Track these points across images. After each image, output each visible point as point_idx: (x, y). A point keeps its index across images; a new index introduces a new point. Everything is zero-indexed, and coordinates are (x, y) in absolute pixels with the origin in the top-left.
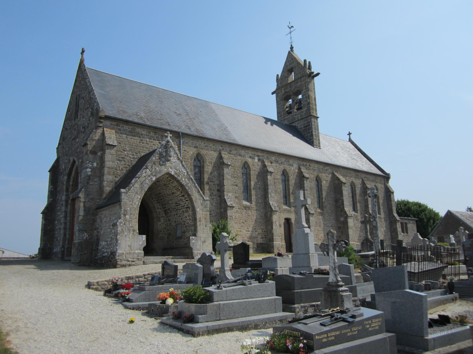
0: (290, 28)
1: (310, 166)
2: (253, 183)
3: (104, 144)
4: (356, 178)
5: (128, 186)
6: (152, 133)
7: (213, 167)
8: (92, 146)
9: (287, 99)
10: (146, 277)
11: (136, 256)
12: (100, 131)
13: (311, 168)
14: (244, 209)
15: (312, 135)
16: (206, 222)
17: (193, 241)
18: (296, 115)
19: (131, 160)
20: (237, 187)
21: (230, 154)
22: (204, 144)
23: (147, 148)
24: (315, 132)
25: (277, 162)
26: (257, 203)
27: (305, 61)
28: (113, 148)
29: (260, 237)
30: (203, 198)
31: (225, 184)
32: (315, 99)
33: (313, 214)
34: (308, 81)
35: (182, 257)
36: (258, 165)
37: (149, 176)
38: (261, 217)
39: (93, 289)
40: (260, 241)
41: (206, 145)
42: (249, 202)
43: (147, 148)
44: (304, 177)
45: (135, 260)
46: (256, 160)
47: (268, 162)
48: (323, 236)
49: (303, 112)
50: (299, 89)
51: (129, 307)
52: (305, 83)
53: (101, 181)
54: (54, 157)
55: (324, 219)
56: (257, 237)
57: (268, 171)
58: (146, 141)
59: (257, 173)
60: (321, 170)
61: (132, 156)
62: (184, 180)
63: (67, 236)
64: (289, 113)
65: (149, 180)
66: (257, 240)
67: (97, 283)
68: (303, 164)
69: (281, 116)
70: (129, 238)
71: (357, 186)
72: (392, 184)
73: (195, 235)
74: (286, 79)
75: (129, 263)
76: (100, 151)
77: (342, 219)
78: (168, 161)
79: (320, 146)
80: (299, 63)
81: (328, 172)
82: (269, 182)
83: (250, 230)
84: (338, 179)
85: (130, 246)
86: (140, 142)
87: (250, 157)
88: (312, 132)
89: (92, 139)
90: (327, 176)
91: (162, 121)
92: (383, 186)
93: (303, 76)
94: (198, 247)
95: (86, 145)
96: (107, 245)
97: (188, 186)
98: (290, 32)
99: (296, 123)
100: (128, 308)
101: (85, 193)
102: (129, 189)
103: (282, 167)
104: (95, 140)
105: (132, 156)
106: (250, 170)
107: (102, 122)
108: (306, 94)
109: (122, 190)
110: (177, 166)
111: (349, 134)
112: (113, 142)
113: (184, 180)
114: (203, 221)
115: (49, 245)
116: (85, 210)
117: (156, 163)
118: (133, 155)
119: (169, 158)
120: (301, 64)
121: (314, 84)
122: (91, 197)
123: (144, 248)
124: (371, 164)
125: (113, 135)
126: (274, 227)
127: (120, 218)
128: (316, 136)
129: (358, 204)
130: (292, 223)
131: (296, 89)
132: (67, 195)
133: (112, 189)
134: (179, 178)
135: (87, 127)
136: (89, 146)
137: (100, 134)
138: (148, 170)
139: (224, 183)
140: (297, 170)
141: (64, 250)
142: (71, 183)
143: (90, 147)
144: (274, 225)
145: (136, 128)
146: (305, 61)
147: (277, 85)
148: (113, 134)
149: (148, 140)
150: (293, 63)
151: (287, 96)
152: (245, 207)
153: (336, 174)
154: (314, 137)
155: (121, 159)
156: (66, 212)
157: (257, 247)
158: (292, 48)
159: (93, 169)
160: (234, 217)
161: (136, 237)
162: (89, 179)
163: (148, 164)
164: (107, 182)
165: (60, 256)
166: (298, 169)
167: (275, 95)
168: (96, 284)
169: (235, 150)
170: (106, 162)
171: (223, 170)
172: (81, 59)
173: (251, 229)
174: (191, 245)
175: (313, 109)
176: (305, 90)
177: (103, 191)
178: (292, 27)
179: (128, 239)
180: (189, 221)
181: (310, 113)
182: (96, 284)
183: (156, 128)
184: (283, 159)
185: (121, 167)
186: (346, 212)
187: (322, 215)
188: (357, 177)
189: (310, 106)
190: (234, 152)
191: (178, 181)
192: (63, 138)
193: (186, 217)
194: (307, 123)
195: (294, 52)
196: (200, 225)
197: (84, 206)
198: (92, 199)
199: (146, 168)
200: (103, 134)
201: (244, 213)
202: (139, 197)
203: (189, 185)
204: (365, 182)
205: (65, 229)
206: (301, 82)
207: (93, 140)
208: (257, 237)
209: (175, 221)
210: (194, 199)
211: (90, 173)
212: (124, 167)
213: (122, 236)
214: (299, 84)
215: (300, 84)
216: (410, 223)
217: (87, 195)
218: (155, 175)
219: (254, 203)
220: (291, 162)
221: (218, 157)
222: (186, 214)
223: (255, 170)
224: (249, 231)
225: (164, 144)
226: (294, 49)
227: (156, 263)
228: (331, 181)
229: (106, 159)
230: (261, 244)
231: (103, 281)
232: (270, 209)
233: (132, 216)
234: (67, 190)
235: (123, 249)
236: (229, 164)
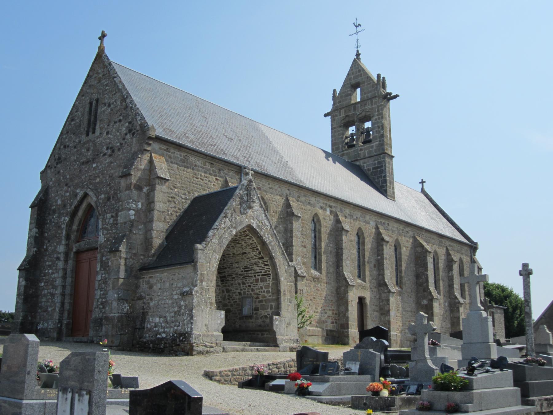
0: (357, 27)
1: (388, 225)
2: (323, 245)
3: (153, 176)
4: (439, 245)
5: (204, 241)
6: (207, 164)
7: (278, 218)
8: (137, 178)
9: (347, 126)
10: (271, 367)
11: (214, 339)
12: (146, 157)
13: (390, 228)
14: (312, 280)
15: (385, 181)
16: (291, 296)
17: (277, 323)
18: (361, 150)
19: (183, 202)
20: (305, 250)
21: (298, 201)
22: (269, 184)
23: (201, 185)
24: (389, 177)
25: (351, 216)
26: (327, 273)
27: (379, 76)
28: (165, 182)
29: (330, 321)
30: (288, 263)
31: (294, 244)
32: (390, 131)
33: (394, 293)
34: (382, 105)
35: (262, 344)
36: (330, 220)
37: (229, 228)
38: (332, 292)
39: (215, 380)
40: (330, 327)
41: (270, 186)
42: (318, 271)
43: (201, 185)
44: (383, 239)
45: (213, 345)
46: (328, 213)
47: (342, 216)
48: (401, 325)
49: (372, 147)
50: (368, 114)
51: (323, 401)
52: (378, 107)
53: (148, 230)
54: (37, 187)
55: (403, 301)
56: (326, 322)
57: (343, 229)
58: (201, 175)
59: (328, 231)
60: (401, 231)
61: (183, 196)
62: (267, 236)
63: (67, 306)
64: (350, 146)
65: (229, 234)
66: (327, 326)
67: (220, 372)
68: (381, 222)
69: (338, 149)
70: (206, 314)
71: (440, 258)
72: (478, 256)
73: (278, 314)
74: (349, 97)
75: (206, 349)
76: (146, 186)
77: (425, 302)
78: (250, 207)
79: (394, 198)
80: (369, 78)
81: (408, 235)
82: (344, 244)
83: (319, 311)
84: (422, 246)
85: (207, 325)
86: (193, 177)
87: (321, 208)
88: (385, 176)
89: (136, 168)
90: (407, 241)
91: (215, 147)
92: (469, 259)
93: (375, 97)
94: (282, 331)
95: (127, 175)
96: (166, 322)
97: (271, 245)
98: (357, 33)
99: (362, 161)
100: (322, 403)
101: (127, 245)
102: (207, 245)
103: (357, 225)
104: (141, 169)
105: (183, 196)
106: (320, 225)
107: (150, 145)
108: (378, 123)
109: (199, 246)
110: (256, 217)
111: (422, 182)
112: (166, 175)
113: (267, 236)
114: (288, 296)
115: (30, 318)
116: (126, 271)
117: (237, 210)
118: (185, 194)
119: (252, 205)
120: (372, 80)
121: (106, 56)
122: (134, 251)
123: (222, 329)
124: (453, 228)
125: (163, 165)
126: (350, 308)
127: (196, 286)
128: (390, 183)
129: (441, 282)
130: (366, 304)
131: (363, 114)
132: (67, 245)
133: (163, 242)
134: (262, 234)
135: (119, 149)
136: (133, 178)
137: (146, 161)
138: (227, 219)
139: (292, 242)
140: (374, 230)
141: (61, 326)
142: (75, 227)
143: (134, 180)
144: (350, 305)
145: (189, 155)
146: (379, 76)
147: (334, 105)
148: (163, 162)
149: (203, 174)
150: (361, 76)
151: (349, 122)
152: (314, 278)
153: (418, 238)
154: (388, 184)
155: (170, 199)
156: (65, 270)
157: (327, 335)
158: (358, 55)
159: (137, 211)
160: (304, 291)
161: (214, 313)
162: (132, 225)
163: (228, 211)
164: (157, 231)
165: (55, 335)
166: (375, 229)
167: (329, 118)
168: (218, 374)
169: (305, 196)
170: (156, 203)
171: (292, 223)
172: (99, 47)
173: (319, 310)
174: (275, 328)
175: (387, 144)
176: (377, 117)
177: (151, 244)
178: (359, 25)
179: (205, 315)
180: (266, 295)
181: (383, 149)
182: (218, 374)
183: (213, 158)
184: (358, 214)
185: (171, 210)
186: (430, 292)
187: (400, 295)
188: (440, 244)
189: (383, 140)
190: (303, 199)
191: (260, 237)
192: (57, 159)
193: (262, 288)
194: (379, 163)
195: (361, 60)
196: (284, 300)
197: (125, 265)
198: (135, 255)
199: (226, 217)
200: (151, 162)
201: (312, 287)
202: (218, 256)
203: (273, 243)
204: (451, 252)
205: (63, 295)
206: (372, 105)
207: (138, 170)
208: (326, 322)
209: (240, 293)
210: (278, 264)
211: (133, 217)
212: (174, 211)
213: (198, 311)
214: (369, 107)
215: (370, 106)
216: (497, 313)
217: (130, 248)
218: (235, 228)
219: (323, 272)
220: (368, 217)
221: (284, 204)
222: (261, 284)
223: (326, 227)
224: (317, 312)
225: (246, 184)
226: (361, 56)
227: (237, 351)
228: (411, 248)
229: (156, 199)
230: (331, 331)
231: (226, 371)
232: (344, 283)
233: (209, 282)
234: (68, 237)
235: (199, 330)
236: (299, 215)
